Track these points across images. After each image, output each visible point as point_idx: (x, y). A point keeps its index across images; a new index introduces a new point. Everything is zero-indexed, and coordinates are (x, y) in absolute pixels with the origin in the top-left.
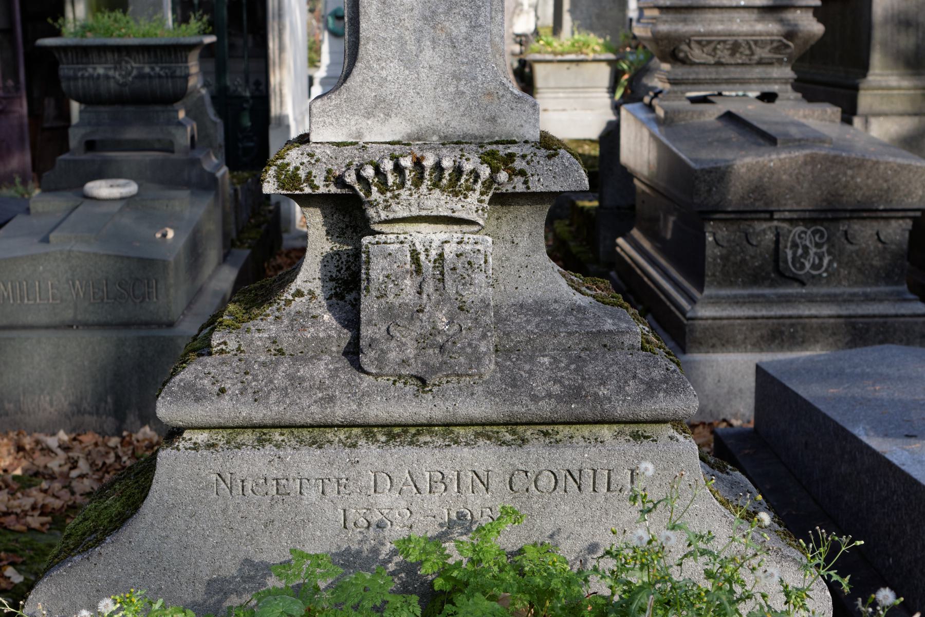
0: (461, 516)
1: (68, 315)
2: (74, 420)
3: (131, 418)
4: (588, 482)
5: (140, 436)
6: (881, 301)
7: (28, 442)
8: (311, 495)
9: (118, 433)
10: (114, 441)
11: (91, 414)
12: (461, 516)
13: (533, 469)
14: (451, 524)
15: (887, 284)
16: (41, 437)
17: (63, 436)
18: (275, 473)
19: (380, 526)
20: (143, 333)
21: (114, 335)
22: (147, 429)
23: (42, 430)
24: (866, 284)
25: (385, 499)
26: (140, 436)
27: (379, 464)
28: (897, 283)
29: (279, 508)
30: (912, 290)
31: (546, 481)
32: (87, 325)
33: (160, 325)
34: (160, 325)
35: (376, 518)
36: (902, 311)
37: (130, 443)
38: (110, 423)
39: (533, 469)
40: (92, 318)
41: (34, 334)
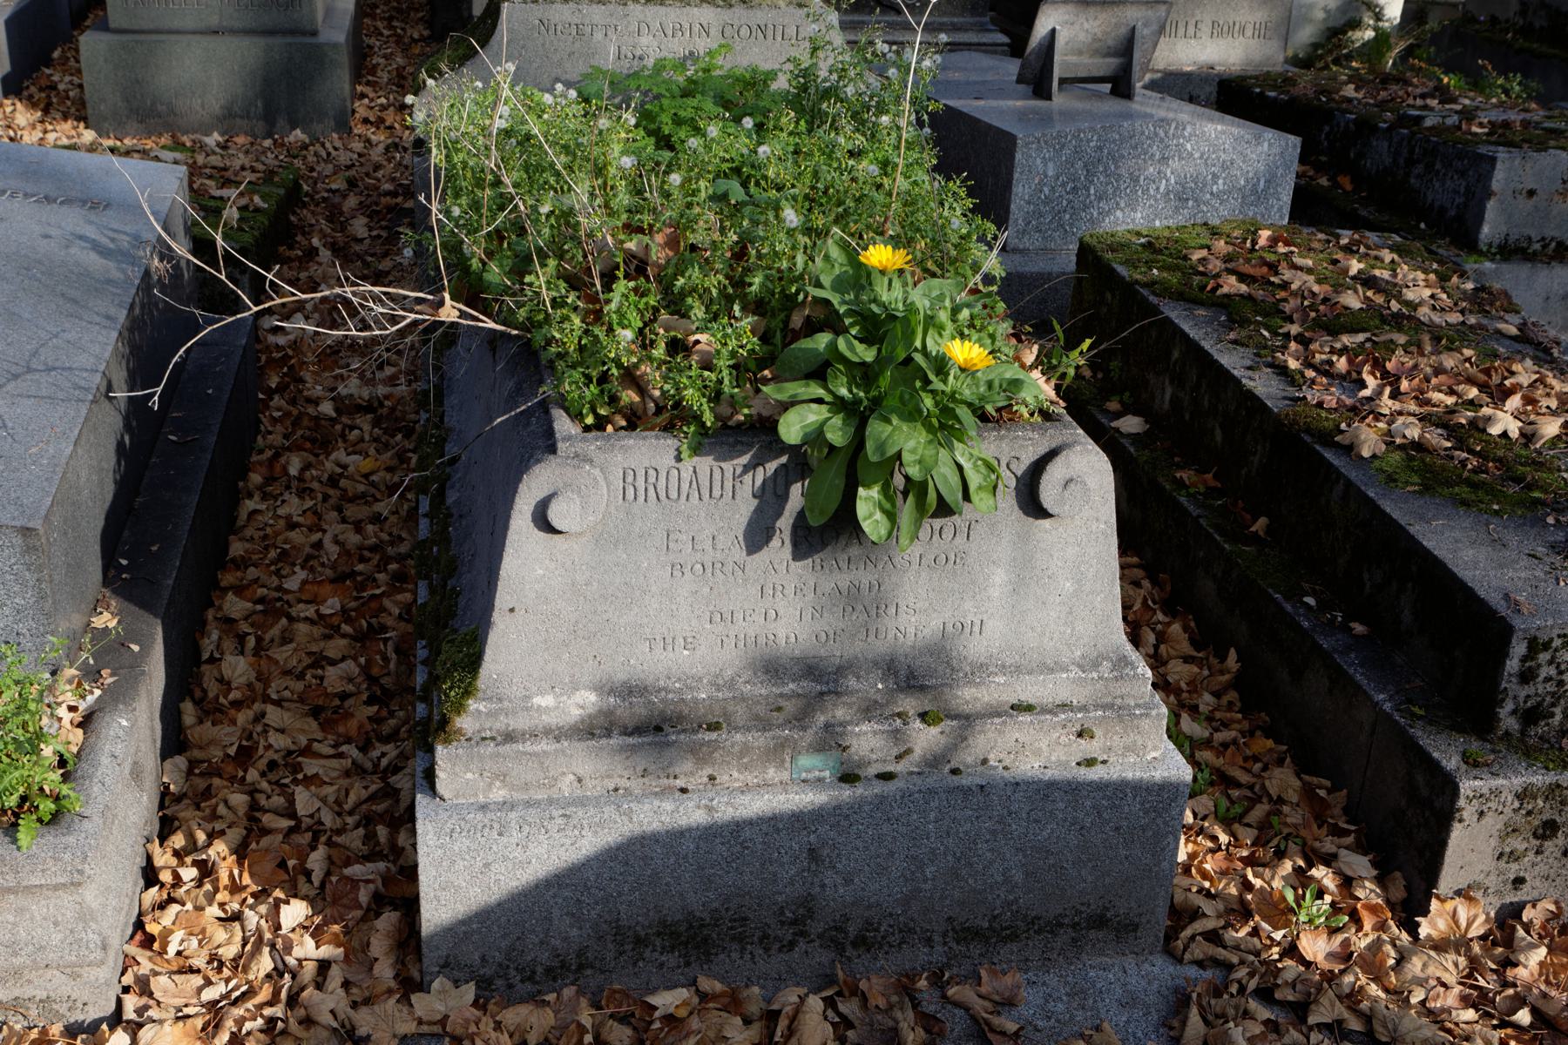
0: (691, 53)
1: (214, 21)
2: (227, 120)
3: (281, 122)
4: (770, 33)
5: (292, 138)
6: (966, 30)
7: (186, 140)
8: (599, 36)
9: (269, 135)
10: (268, 143)
11: (242, 117)
12: (691, 53)
13: (736, 23)
14: (685, 58)
15: (972, 15)
16: (197, 136)
17: (216, 136)
18: (577, 21)
19: (641, 58)
20: (289, 40)
21: (261, 42)
22: (298, 131)
23: (195, 132)
24: (954, 15)
25: (645, 40)
26: (292, 138)
27: (641, 17)
28: (981, 15)
29: (577, 45)
30: (993, 21)
31: (744, 31)
32: (233, 32)
33: (304, 33)
34: (304, 33)
35: (638, 53)
36: (984, 40)
37: (283, 145)
38: (260, 126)
39: (736, 23)
40: (237, 25)
41: (185, 39)
